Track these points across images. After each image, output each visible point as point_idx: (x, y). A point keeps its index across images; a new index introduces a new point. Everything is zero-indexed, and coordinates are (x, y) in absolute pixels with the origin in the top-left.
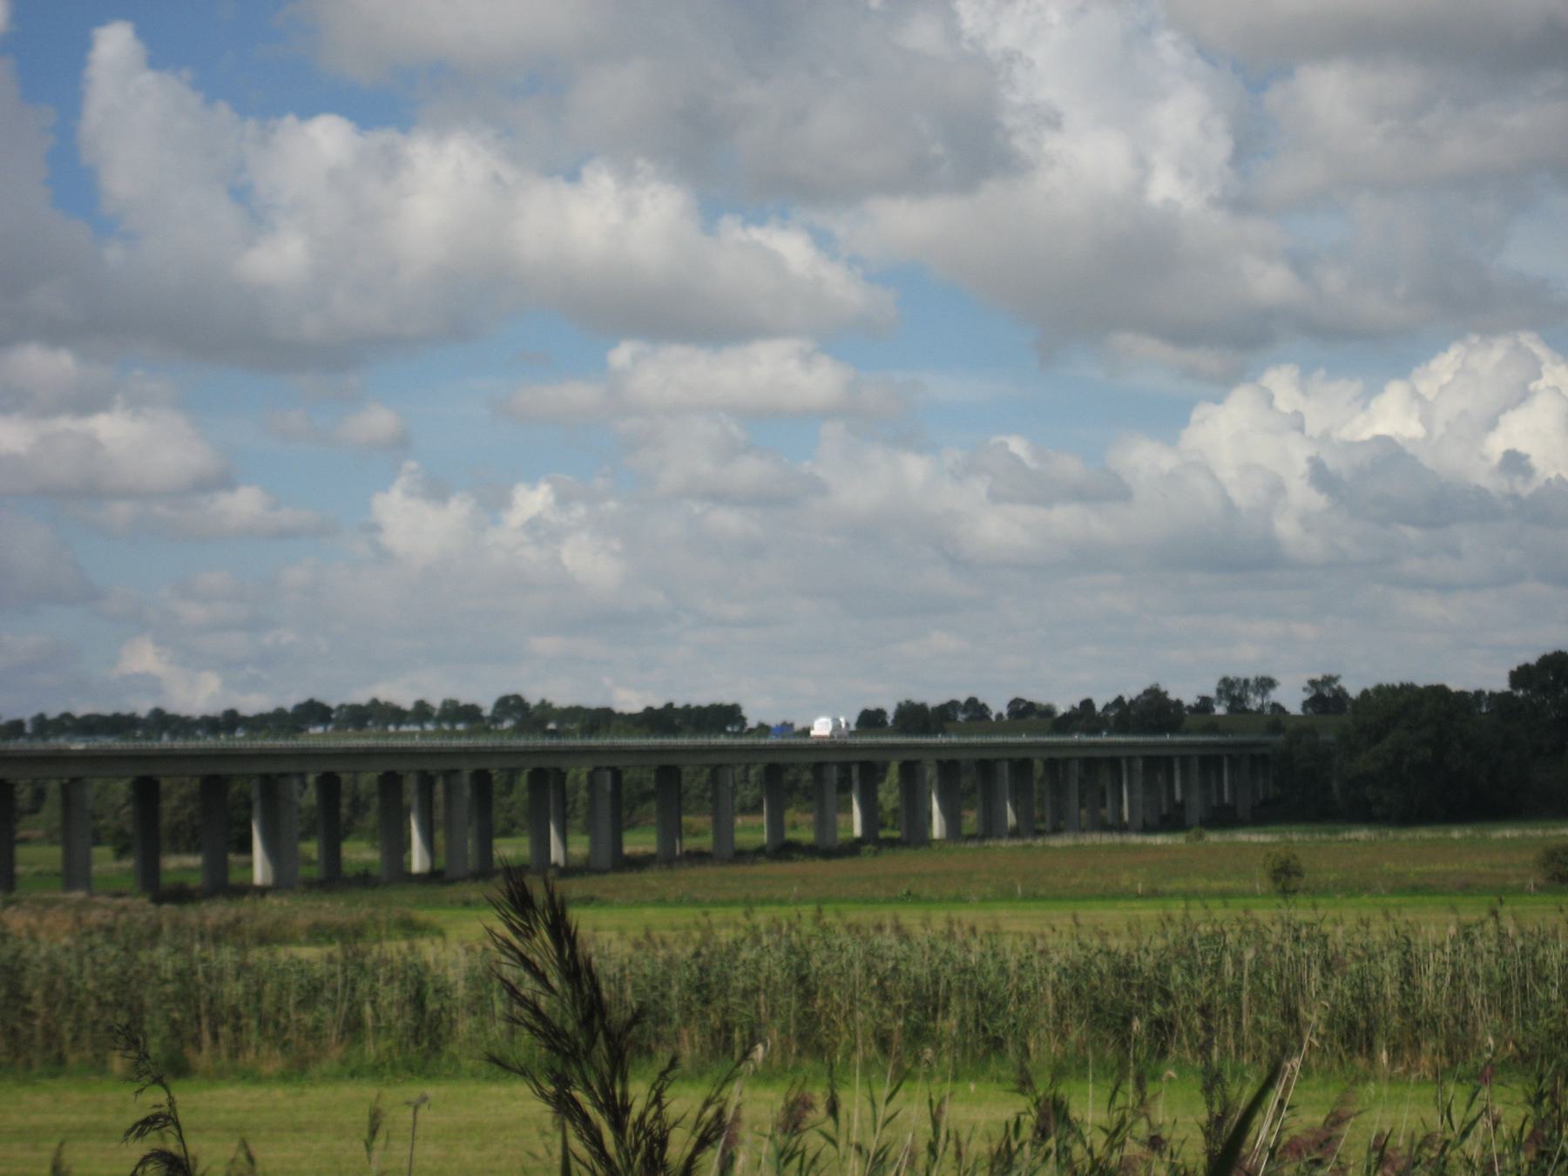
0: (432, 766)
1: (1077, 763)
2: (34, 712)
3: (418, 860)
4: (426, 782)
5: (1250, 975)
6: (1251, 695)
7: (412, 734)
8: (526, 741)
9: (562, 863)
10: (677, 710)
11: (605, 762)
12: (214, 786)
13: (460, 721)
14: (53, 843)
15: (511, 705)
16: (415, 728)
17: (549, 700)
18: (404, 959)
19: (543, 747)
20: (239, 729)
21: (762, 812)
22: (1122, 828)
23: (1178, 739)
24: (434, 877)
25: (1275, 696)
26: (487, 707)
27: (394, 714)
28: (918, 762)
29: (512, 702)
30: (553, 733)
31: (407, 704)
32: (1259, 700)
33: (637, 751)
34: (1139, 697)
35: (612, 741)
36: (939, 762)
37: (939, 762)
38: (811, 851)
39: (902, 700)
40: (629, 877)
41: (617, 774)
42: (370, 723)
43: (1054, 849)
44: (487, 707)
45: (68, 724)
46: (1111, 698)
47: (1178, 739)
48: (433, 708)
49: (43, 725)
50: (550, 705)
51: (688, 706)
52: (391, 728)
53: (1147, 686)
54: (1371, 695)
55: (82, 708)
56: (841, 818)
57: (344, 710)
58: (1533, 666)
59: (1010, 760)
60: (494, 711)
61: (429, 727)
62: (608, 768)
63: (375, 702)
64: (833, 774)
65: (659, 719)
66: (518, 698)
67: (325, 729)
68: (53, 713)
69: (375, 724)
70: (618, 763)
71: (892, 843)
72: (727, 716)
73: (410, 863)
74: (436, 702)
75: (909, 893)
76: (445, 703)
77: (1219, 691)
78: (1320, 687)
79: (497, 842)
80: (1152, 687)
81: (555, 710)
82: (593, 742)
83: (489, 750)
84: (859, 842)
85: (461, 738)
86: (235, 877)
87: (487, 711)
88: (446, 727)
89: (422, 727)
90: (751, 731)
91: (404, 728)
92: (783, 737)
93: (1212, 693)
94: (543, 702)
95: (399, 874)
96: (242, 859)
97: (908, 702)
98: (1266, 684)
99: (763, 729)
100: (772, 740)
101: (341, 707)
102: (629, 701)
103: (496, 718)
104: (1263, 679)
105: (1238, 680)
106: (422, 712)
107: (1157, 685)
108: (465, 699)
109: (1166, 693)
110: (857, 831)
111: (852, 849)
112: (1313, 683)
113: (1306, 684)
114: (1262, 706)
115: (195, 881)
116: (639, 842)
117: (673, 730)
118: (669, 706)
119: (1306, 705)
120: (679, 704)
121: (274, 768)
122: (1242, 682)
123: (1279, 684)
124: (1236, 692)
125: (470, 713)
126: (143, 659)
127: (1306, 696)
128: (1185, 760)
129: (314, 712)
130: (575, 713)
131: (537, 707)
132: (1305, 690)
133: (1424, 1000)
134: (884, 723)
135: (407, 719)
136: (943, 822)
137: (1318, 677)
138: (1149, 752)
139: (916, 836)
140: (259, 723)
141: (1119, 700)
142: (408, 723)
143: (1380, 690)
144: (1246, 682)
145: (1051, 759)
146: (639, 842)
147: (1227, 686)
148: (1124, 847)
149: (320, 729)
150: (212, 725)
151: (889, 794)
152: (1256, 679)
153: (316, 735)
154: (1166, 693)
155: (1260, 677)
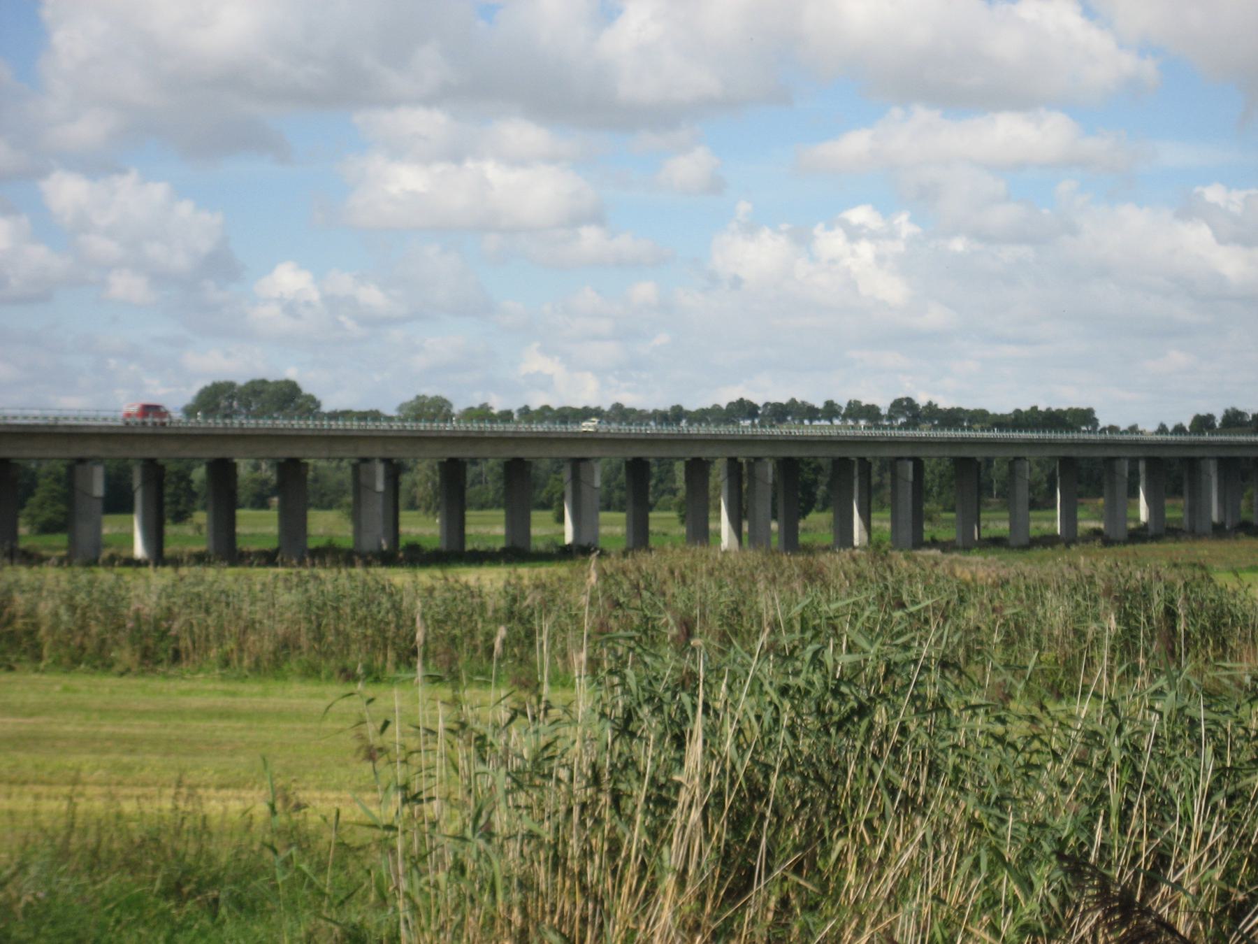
0: (742, 454)
2: (521, 405)
4: (735, 469)
7: (822, 427)
11: (378, 451)
13: (862, 418)
14: (499, 506)
15: (904, 406)
18: (686, 605)
19: (962, 438)
21: (1054, 507)
26: (884, 405)
27: (811, 413)
29: (905, 403)
31: (820, 405)
39: (1229, 407)
41: (918, 463)
42: (789, 418)
44: (884, 405)
48: (840, 407)
60: (890, 411)
61: (837, 422)
62: (910, 459)
63: (793, 401)
66: (909, 400)
68: (535, 405)
70: (396, 452)
72: (1086, 417)
76: (850, 403)
79: (471, 515)
85: (862, 428)
87: (884, 411)
88: (850, 422)
91: (816, 423)
94: (930, 403)
97: (1233, 409)
99: (1113, 429)
101: (766, 405)
102: (1001, 405)
106: (830, 410)
108: (865, 402)
111: (1139, 535)
118: (1034, 409)
125: (871, 413)
126: (535, 363)
129: (744, 409)
131: (825, 407)
134: (1213, 425)
138: (1223, 454)
140: (702, 416)
142: (819, 419)
145: (452, 461)
149: (748, 422)
150: (662, 417)
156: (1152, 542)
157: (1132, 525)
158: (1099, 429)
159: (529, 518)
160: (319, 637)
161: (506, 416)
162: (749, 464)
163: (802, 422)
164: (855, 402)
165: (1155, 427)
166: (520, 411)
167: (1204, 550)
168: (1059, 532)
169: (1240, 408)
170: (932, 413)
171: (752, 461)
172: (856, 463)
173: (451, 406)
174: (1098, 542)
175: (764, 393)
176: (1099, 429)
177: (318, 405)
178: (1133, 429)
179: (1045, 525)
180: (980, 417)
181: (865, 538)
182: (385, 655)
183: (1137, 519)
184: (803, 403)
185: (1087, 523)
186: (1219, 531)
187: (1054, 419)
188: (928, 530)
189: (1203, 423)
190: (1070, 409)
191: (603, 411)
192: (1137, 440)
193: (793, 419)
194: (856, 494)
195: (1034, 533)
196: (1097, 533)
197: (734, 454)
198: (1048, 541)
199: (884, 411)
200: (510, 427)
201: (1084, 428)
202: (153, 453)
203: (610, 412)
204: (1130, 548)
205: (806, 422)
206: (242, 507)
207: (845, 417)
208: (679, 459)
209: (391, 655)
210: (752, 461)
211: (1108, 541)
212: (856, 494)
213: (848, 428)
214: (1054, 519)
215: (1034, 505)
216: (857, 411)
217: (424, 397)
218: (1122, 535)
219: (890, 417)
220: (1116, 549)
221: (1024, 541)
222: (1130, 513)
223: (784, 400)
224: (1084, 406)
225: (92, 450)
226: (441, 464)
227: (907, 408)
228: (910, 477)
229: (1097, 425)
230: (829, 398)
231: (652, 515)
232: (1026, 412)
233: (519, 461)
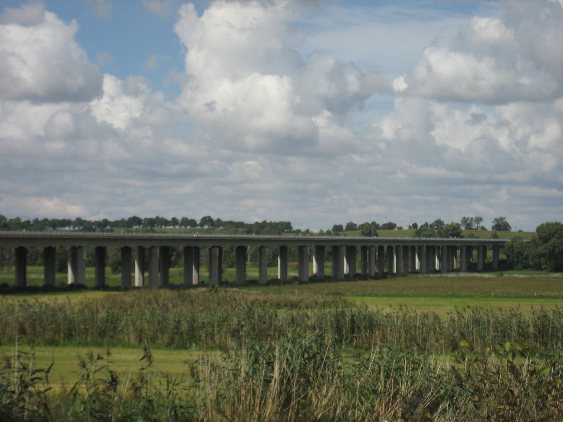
0: (147, 245)
1: (465, 247)
2: (34, 218)
4: (142, 250)
6: (474, 223)
11: (216, 244)
15: (207, 220)
16: (172, 227)
17: (220, 219)
20: (108, 226)
21: (277, 265)
22: (457, 271)
23: (458, 239)
25: (482, 224)
26: (198, 219)
27: (165, 222)
28: (305, 246)
29: (207, 219)
30: (108, 231)
31: (169, 218)
32: (476, 225)
34: (433, 223)
35: (152, 234)
37: (317, 246)
39: (349, 222)
41: (221, 249)
42: (156, 225)
43: (450, 278)
44: (198, 219)
46: (423, 223)
47: (458, 239)
48: (179, 221)
50: (221, 220)
51: (271, 222)
52: (163, 227)
53: (436, 219)
54: (545, 226)
57: (147, 220)
59: (465, 246)
60: (201, 222)
61: (177, 227)
62: (217, 247)
65: (262, 227)
66: (209, 217)
72: (287, 226)
74: (179, 218)
76: (183, 219)
77: (462, 221)
78: (498, 221)
80: (438, 220)
82: (280, 237)
87: (198, 222)
88: (183, 227)
90: (294, 232)
91: (168, 227)
92: (420, 236)
93: (460, 222)
98: (479, 220)
99: (298, 231)
100: (300, 236)
101: (146, 219)
102: (251, 219)
103: (202, 225)
104: (478, 217)
105: (469, 218)
106: (174, 222)
107: (440, 219)
108: (190, 218)
109: (443, 222)
112: (496, 220)
113: (493, 220)
114: (478, 227)
118: (265, 222)
119: (493, 227)
120: (268, 221)
122: (471, 219)
123: (483, 220)
124: (468, 222)
125: (192, 223)
127: (493, 224)
128: (420, 248)
129: (135, 221)
132: (493, 222)
133: (383, 405)
137: (498, 218)
140: (117, 224)
141: (415, 226)
142: (169, 226)
143: (548, 224)
144: (472, 219)
146: (253, 273)
147: (465, 220)
148: (459, 278)
152: (476, 218)
154: (452, 223)
155: (477, 217)
156: (319, 283)
157: (310, 275)
158: (292, 231)
160: (34, 329)
167: (342, 286)
168: (279, 277)
169: (354, 222)
170: (219, 223)
171: (539, 408)
174: (297, 283)
176: (292, 231)
178: (307, 231)
179: (273, 274)
180: (240, 225)
182: (59, 336)
183: (313, 272)
185: (292, 273)
186: (347, 278)
188: (225, 277)
189: (338, 229)
190: (280, 222)
193: (158, 226)
194: (193, 260)
195: (269, 278)
196: (296, 278)
198: (274, 282)
199: (198, 222)
201: (286, 231)
203: (75, 222)
204: (310, 285)
207: (181, 225)
209: (62, 335)
210: (539, 408)
211: (301, 282)
212: (193, 260)
214: (277, 272)
215: (269, 265)
216: (186, 222)
218: (306, 279)
220: (304, 286)
221: (265, 282)
222: (310, 270)
223: (153, 216)
224: (286, 221)
227: (208, 221)
228: (217, 254)
229: (292, 229)
232: (261, 223)
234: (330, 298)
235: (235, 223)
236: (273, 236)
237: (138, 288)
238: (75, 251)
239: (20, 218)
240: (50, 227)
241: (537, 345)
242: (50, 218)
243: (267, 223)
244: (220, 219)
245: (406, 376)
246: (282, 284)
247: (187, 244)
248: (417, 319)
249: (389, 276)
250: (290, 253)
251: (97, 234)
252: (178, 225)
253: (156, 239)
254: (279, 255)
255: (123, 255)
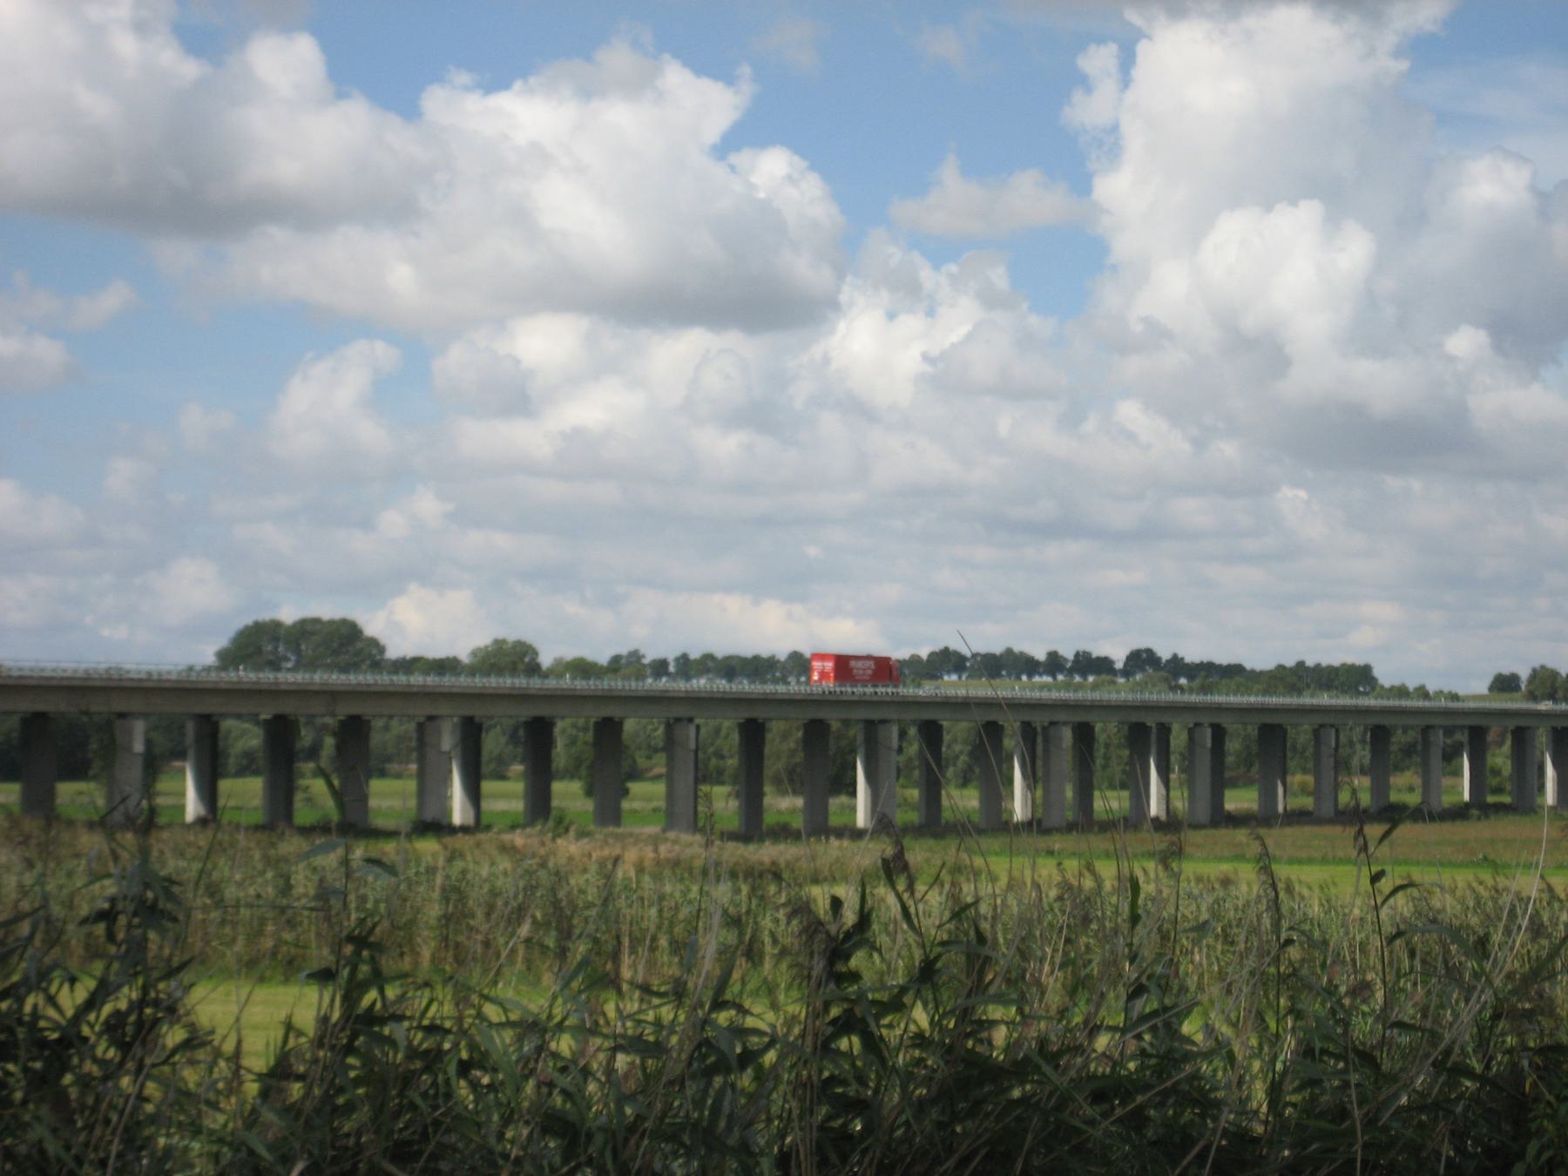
0: (1039, 720)
2: (678, 653)
3: (1019, 806)
4: (1028, 732)
5: (645, 940)
8: (1048, 694)
9: (1163, 817)
10: (1308, 668)
11: (1328, 720)
12: (816, 731)
15: (1141, 660)
16: (1047, 679)
24: (1034, 826)
26: (1119, 656)
27: (1028, 665)
28: (1529, 728)
31: (1040, 655)
33: (1061, 706)
36: (1554, 729)
37: (1554, 729)
38: (1418, 814)
39: (1537, 665)
40: (1224, 834)
44: (1119, 656)
45: (708, 665)
48: (1066, 660)
49: (687, 666)
50: (1182, 659)
51: (1318, 665)
55: (722, 648)
56: (1447, 782)
58: (602, 667)
60: (1126, 664)
63: (1009, 651)
64: (783, 741)
66: (1149, 651)
67: (960, 678)
69: (1009, 675)
71: (1500, 808)
72: (1359, 677)
73: (1011, 812)
74: (1068, 653)
75: (1485, 858)
76: (1077, 655)
81: (1187, 665)
82: (1209, 698)
83: (1088, 703)
84: (1467, 806)
86: (834, 821)
87: (1119, 665)
88: (1078, 679)
89: (1055, 678)
91: (1037, 679)
94: (1175, 656)
95: (996, 823)
96: (844, 799)
97: (1543, 667)
99: (1402, 692)
102: (1260, 658)
106: (1054, 663)
110: (1466, 797)
111: (1459, 813)
115: (798, 823)
116: (1239, 800)
117: (1295, 689)
118: (1301, 664)
120: (1310, 662)
121: (875, 715)
125: (1102, 666)
130: (307, 628)
135: (1041, 670)
136: (869, 792)
139: (1524, 804)
142: (1041, 675)
146: (1239, 800)
149: (954, 677)
151: (1501, 758)
153: (952, 685)
159: (1223, 795)
161: (660, 667)
162: (1044, 729)
163: (1019, 678)
164: (1084, 652)
165: (1480, 686)
166: (677, 660)
170: (1177, 666)
172: (1154, 730)
173: (535, 653)
175: (985, 638)
177: (382, 650)
181: (202, 811)
184: (1021, 653)
187: (1326, 677)
189: (1504, 684)
190: (1343, 665)
191: (778, 661)
192: (1356, 706)
197: (1026, 718)
199: (1119, 665)
200: (663, 683)
202: (1216, 720)
203: (786, 661)
205: (1024, 678)
206: (486, 778)
207: (1070, 672)
208: (1065, 723)
213: (1078, 687)
216: (1088, 664)
217: (504, 641)
219: (1126, 672)
223: (997, 648)
224: (1359, 660)
225: (1061, 716)
226: (740, 725)
228: (1209, 743)
230: (1052, 648)
231: (376, 785)
233: (40, 717)
234: (1152, 875)
235: (1220, 666)
236: (1252, 699)
237: (464, 829)
238: (871, 726)
239: (642, 651)
240: (722, 677)
241: (1294, 1105)
242: (720, 651)
243: (1308, 669)
244: (1180, 656)
245: (811, 1140)
246: (1096, 829)
247: (27, 705)
248: (156, 1045)
249: (1475, 812)
250: (1294, 748)
251: (744, 686)
252: (1065, 672)
253: (681, 699)
254: (191, 753)
255: (598, 742)
